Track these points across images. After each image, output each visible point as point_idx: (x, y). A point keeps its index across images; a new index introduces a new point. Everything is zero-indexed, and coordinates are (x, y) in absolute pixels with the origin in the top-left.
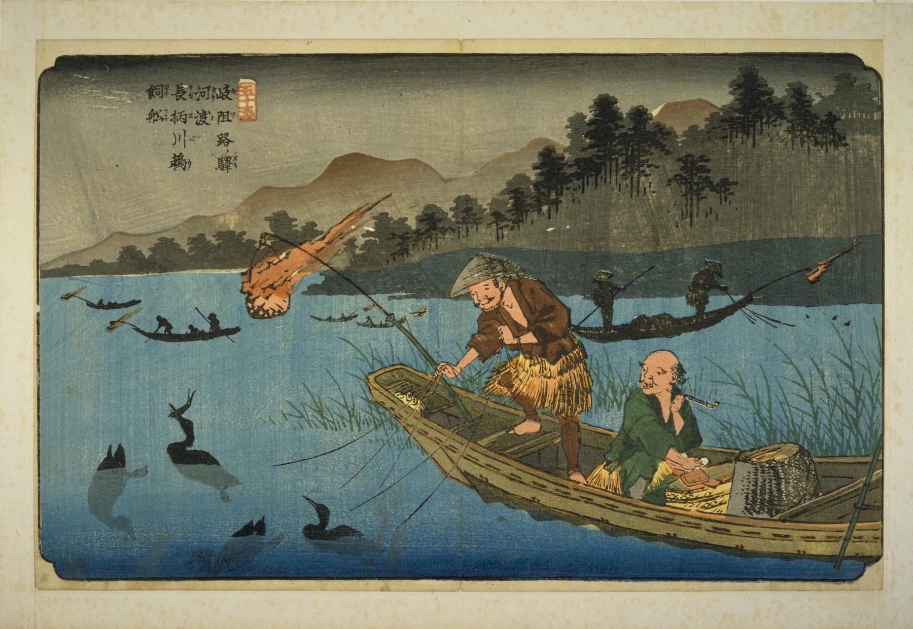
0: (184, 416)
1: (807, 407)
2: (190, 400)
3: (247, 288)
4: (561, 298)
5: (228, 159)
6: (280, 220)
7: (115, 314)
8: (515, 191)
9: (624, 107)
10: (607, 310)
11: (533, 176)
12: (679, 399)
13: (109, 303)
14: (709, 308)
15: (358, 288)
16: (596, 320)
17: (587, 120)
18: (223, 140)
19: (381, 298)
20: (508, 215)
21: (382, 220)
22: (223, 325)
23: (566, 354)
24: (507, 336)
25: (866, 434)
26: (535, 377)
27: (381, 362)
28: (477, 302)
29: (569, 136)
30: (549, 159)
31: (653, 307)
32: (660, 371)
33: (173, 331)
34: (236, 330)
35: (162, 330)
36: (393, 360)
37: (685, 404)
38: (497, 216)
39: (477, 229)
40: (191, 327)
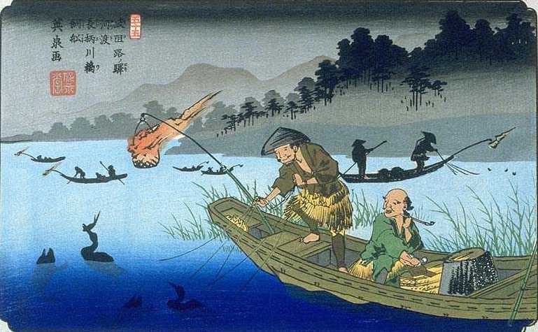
0: (92, 230)
1: (489, 226)
2: (96, 221)
3: (132, 148)
4: (332, 156)
5: (120, 66)
6: (153, 105)
7: (49, 165)
8: (304, 87)
9: (374, 35)
10: (361, 163)
11: (315, 79)
12: (408, 221)
13: (46, 158)
14: (427, 163)
15: (205, 150)
16: (355, 171)
17: (350, 44)
18: (118, 53)
19: (218, 156)
20: (299, 104)
21: (219, 105)
22: (117, 174)
23: (336, 191)
24: (299, 179)
25: (526, 244)
26: (318, 209)
27: (218, 196)
28: (279, 158)
29: (339, 54)
30: (325, 67)
31: (390, 163)
32: (396, 202)
33: (86, 177)
34: (125, 176)
35: (79, 176)
36: (227, 195)
37: (412, 224)
38: (292, 104)
39: (279, 112)
40: (97, 174)
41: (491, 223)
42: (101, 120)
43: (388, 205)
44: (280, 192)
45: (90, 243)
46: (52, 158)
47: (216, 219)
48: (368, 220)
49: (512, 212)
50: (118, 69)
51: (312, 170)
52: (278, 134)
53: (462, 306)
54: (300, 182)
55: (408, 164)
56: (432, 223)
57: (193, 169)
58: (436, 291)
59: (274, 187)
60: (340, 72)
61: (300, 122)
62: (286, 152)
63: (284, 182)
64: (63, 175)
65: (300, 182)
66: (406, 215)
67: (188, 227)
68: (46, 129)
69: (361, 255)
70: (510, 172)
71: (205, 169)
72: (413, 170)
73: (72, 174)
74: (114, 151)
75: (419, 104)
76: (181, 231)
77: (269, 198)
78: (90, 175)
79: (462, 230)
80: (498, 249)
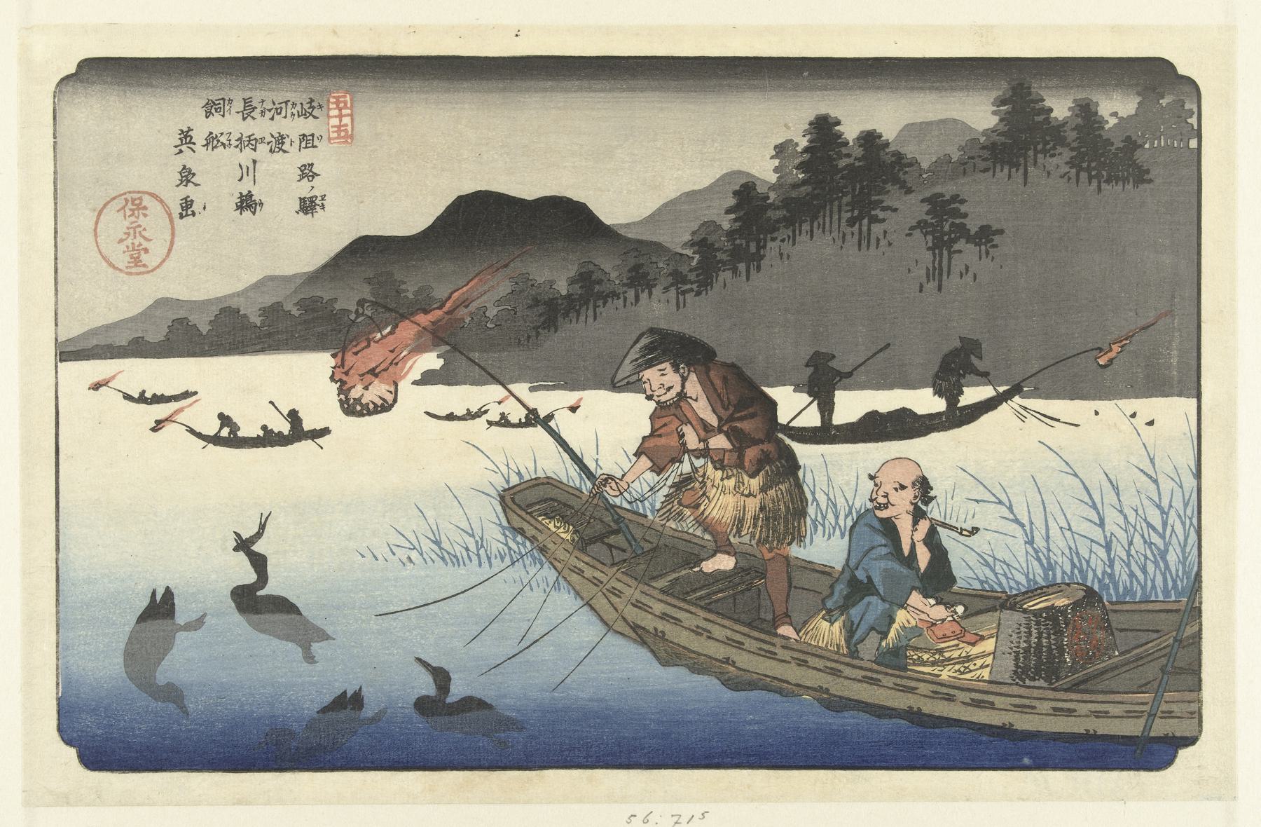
1: (1097, 534)
2: (263, 527)
5: (312, 200)
9: (850, 130)
10: (827, 408)
12: (924, 526)
18: (307, 172)
19: (521, 389)
20: (692, 277)
26: (729, 499)
27: (519, 474)
28: (649, 393)
30: (746, 195)
31: (887, 401)
34: (325, 431)
35: (225, 432)
37: (932, 532)
41: (1102, 524)
42: (273, 312)
43: (881, 493)
44: (650, 464)
45: (250, 577)
46: (166, 394)
47: (518, 523)
48: (837, 523)
49: (1146, 502)
50: (308, 206)
51: (720, 419)
52: (645, 341)
53: (1045, 706)
54: (692, 441)
55: (926, 401)
56: (975, 530)
57: (470, 416)
58: (986, 674)
59: (638, 454)
60: (778, 208)
61: (696, 317)
62: (663, 378)
63: (656, 451)
64: (192, 431)
65: (692, 441)
66: (918, 515)
67: (455, 540)
68: (459, 413)
69: (823, 601)
70: (1140, 421)
71: (494, 415)
72: (939, 414)
73: (212, 427)
74: (300, 379)
75: (945, 277)
76: (437, 543)
77: (628, 478)
78: (249, 429)
79: (1040, 542)
80: (1116, 589)
